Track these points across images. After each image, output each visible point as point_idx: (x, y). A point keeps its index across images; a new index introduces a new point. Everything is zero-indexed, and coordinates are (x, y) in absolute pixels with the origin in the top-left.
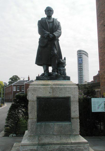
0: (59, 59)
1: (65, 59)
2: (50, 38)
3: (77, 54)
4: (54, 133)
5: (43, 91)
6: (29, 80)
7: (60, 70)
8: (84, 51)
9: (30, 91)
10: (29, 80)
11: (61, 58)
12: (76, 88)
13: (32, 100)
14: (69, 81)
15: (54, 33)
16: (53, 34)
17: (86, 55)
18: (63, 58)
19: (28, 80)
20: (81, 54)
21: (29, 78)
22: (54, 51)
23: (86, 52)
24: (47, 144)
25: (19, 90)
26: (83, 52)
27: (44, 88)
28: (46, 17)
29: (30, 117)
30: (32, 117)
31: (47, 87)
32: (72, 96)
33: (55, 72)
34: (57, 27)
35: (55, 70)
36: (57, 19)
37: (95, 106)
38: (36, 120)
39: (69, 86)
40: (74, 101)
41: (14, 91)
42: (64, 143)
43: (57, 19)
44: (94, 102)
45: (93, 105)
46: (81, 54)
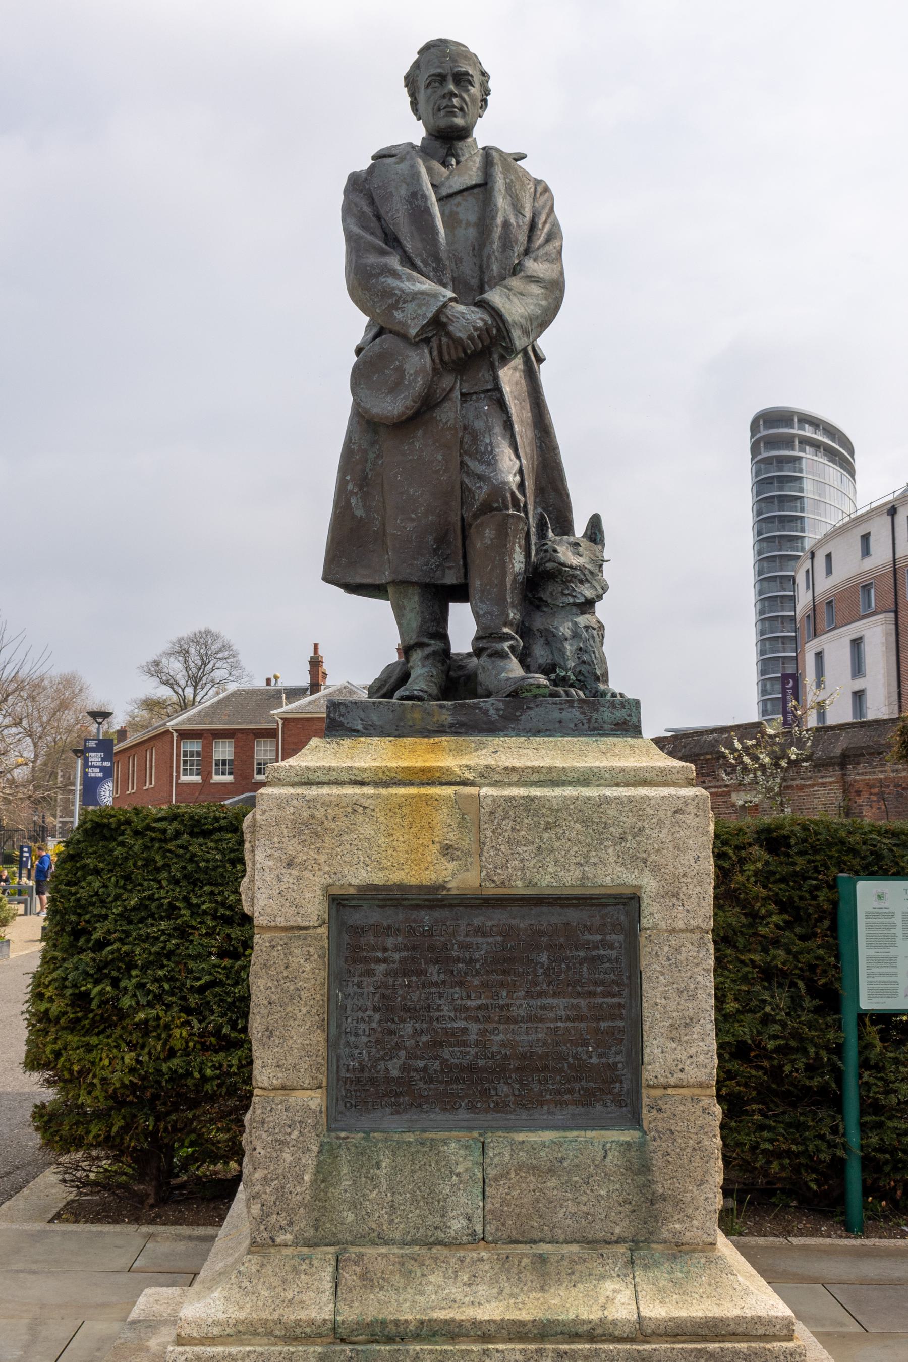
0: (542, 534)
1: (595, 524)
2: (458, 342)
3: (755, 449)
4: (479, 1228)
5: (382, 840)
6: (315, 686)
7: (551, 638)
8: (815, 423)
9: (270, 836)
10: (315, 686)
11: (565, 526)
12: (691, 808)
13: (281, 921)
14: (631, 741)
15: (495, 297)
16: (484, 305)
17: (831, 454)
18: (580, 527)
19: (304, 680)
20: (788, 442)
21: (315, 664)
22: (490, 459)
23: (831, 431)
24: (412, 1327)
25: (229, 779)
26: (808, 432)
27: (395, 808)
28: (418, 142)
29: (266, 1071)
30: (280, 1078)
31: (428, 799)
32: (649, 884)
33: (502, 655)
34: (522, 237)
35: (507, 637)
36: (521, 157)
37: (893, 952)
38: (316, 1100)
39: (623, 792)
40: (673, 931)
41: (184, 779)
42: (576, 1321)
43: (521, 157)
44: (877, 915)
45: (869, 946)
46: (788, 442)
